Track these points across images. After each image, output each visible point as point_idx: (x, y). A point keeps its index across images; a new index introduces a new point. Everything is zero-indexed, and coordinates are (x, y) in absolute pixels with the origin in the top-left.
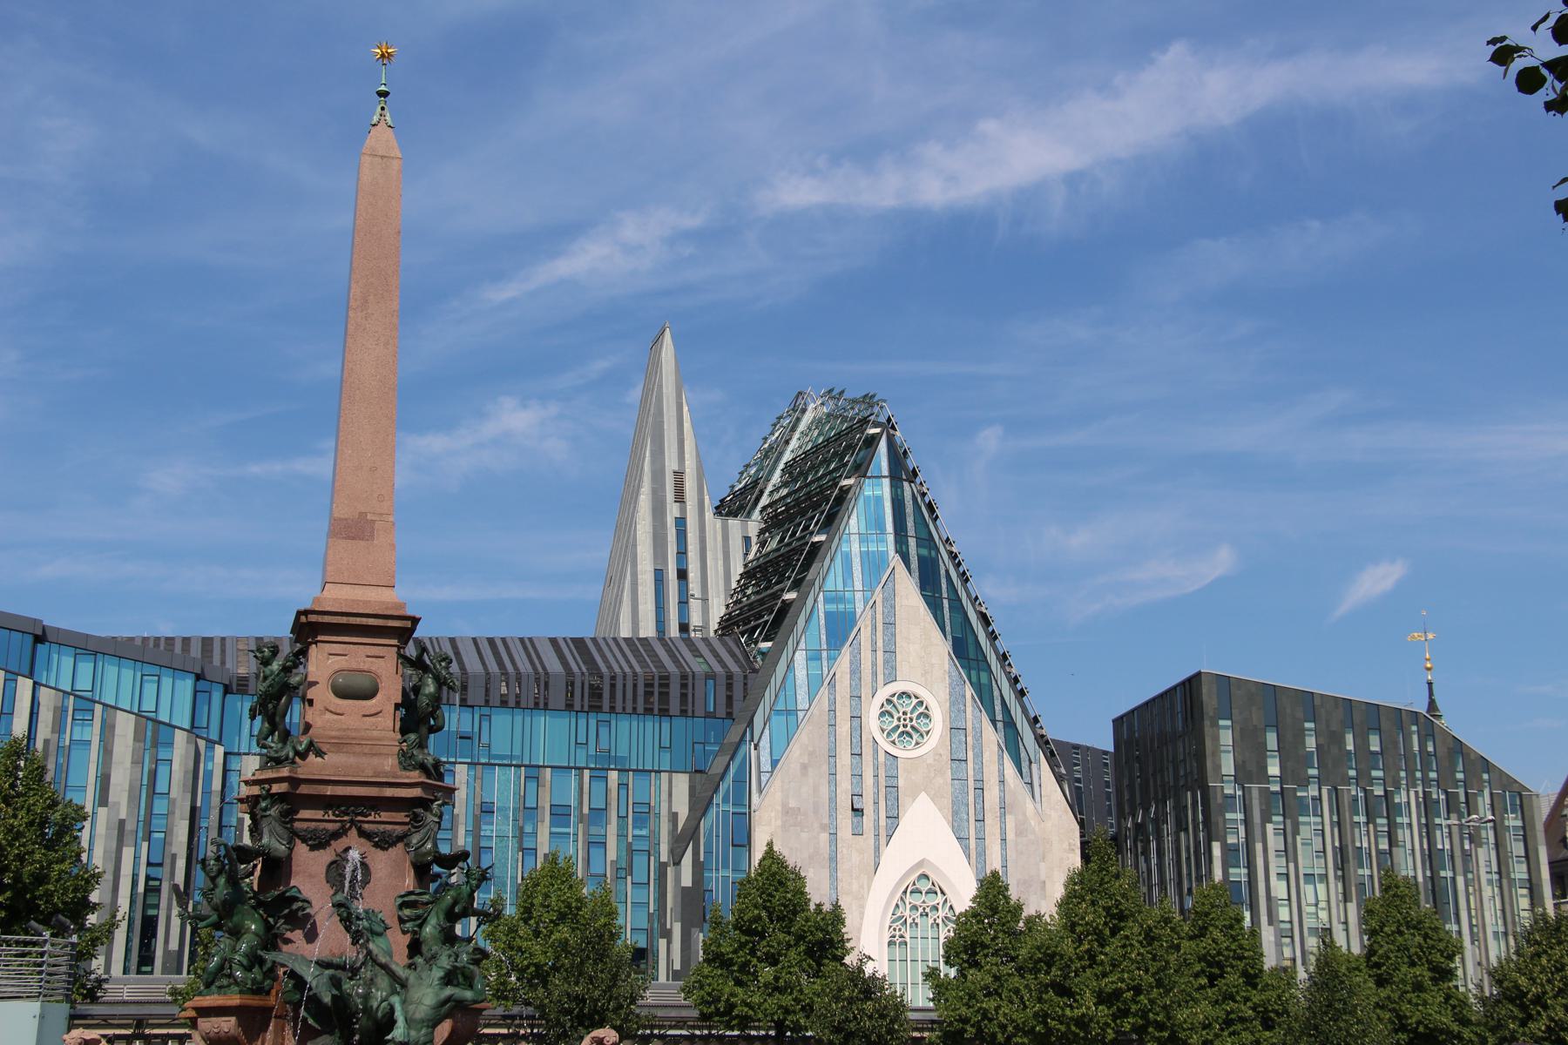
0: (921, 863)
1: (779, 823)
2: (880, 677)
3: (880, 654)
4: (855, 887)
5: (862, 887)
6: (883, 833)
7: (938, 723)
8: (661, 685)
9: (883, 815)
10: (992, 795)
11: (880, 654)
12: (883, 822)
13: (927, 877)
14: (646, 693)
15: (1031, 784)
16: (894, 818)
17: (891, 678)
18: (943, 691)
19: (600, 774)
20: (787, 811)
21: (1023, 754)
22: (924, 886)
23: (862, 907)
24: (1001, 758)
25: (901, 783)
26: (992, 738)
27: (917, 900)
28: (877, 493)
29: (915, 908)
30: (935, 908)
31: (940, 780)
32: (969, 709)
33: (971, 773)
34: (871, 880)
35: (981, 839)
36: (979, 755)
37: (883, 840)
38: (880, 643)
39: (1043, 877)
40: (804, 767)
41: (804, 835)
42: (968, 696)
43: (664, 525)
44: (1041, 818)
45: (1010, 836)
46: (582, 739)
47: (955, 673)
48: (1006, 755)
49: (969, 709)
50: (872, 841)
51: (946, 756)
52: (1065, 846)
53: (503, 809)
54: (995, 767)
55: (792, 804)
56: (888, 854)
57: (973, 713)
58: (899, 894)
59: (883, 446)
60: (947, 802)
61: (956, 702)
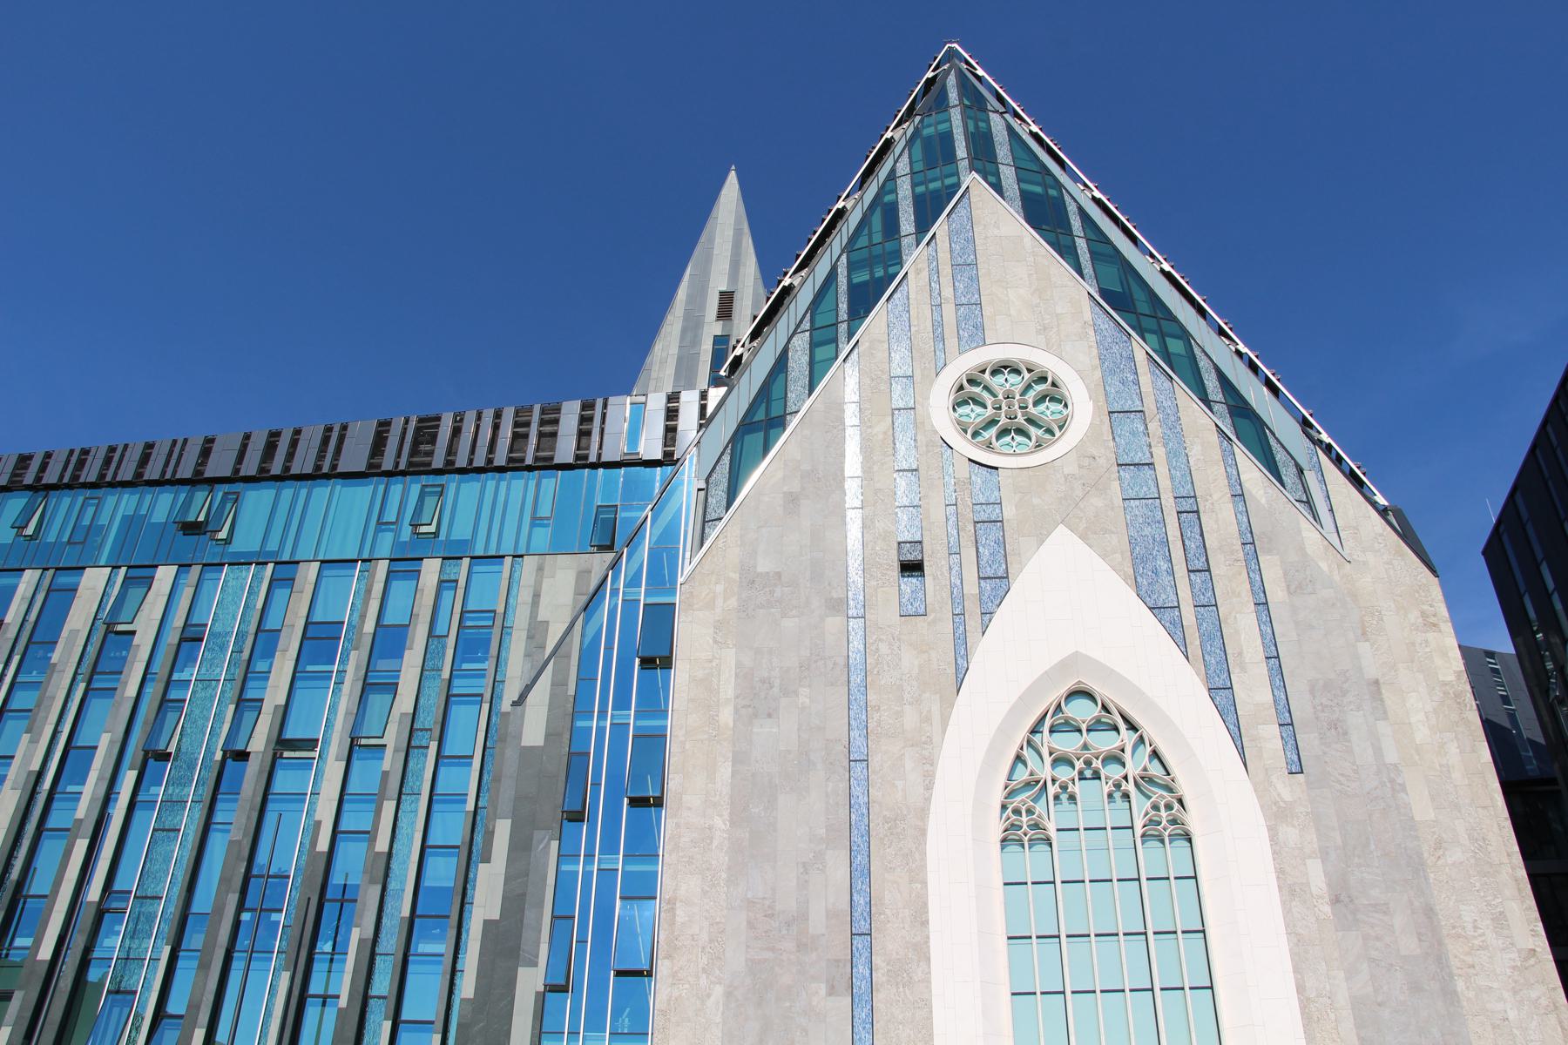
0: (1065, 665)
1: (733, 602)
2: (952, 342)
3: (949, 311)
4: (910, 718)
5: (927, 719)
6: (973, 609)
7: (1083, 409)
8: (542, 423)
9: (971, 574)
10: (1220, 521)
11: (949, 311)
12: (971, 586)
13: (1089, 695)
14: (516, 436)
15: (1309, 503)
16: (997, 581)
17: (976, 335)
18: (1087, 353)
19: (405, 565)
20: (750, 579)
21: (1280, 456)
22: (1082, 711)
23: (928, 765)
24: (1229, 459)
25: (1009, 512)
26: (1201, 425)
27: (1068, 743)
28: (942, 127)
29: (1061, 760)
30: (1115, 758)
31: (1096, 502)
32: (1145, 378)
33: (1165, 483)
34: (948, 706)
35: (1208, 605)
36: (1178, 453)
37: (973, 623)
38: (948, 292)
39: (1372, 672)
40: (792, 500)
41: (789, 624)
42: (1140, 356)
43: (696, 342)
44: (1336, 548)
45: (1276, 594)
46: (391, 516)
47: (1105, 324)
48: (1240, 451)
49: (1145, 378)
50: (948, 627)
51: (1105, 456)
52: (1414, 616)
53: (219, 638)
54: (1219, 471)
55: (764, 565)
56: (988, 652)
57: (1150, 381)
58: (1022, 734)
59: (952, 81)
60: (1118, 540)
61: (1114, 368)
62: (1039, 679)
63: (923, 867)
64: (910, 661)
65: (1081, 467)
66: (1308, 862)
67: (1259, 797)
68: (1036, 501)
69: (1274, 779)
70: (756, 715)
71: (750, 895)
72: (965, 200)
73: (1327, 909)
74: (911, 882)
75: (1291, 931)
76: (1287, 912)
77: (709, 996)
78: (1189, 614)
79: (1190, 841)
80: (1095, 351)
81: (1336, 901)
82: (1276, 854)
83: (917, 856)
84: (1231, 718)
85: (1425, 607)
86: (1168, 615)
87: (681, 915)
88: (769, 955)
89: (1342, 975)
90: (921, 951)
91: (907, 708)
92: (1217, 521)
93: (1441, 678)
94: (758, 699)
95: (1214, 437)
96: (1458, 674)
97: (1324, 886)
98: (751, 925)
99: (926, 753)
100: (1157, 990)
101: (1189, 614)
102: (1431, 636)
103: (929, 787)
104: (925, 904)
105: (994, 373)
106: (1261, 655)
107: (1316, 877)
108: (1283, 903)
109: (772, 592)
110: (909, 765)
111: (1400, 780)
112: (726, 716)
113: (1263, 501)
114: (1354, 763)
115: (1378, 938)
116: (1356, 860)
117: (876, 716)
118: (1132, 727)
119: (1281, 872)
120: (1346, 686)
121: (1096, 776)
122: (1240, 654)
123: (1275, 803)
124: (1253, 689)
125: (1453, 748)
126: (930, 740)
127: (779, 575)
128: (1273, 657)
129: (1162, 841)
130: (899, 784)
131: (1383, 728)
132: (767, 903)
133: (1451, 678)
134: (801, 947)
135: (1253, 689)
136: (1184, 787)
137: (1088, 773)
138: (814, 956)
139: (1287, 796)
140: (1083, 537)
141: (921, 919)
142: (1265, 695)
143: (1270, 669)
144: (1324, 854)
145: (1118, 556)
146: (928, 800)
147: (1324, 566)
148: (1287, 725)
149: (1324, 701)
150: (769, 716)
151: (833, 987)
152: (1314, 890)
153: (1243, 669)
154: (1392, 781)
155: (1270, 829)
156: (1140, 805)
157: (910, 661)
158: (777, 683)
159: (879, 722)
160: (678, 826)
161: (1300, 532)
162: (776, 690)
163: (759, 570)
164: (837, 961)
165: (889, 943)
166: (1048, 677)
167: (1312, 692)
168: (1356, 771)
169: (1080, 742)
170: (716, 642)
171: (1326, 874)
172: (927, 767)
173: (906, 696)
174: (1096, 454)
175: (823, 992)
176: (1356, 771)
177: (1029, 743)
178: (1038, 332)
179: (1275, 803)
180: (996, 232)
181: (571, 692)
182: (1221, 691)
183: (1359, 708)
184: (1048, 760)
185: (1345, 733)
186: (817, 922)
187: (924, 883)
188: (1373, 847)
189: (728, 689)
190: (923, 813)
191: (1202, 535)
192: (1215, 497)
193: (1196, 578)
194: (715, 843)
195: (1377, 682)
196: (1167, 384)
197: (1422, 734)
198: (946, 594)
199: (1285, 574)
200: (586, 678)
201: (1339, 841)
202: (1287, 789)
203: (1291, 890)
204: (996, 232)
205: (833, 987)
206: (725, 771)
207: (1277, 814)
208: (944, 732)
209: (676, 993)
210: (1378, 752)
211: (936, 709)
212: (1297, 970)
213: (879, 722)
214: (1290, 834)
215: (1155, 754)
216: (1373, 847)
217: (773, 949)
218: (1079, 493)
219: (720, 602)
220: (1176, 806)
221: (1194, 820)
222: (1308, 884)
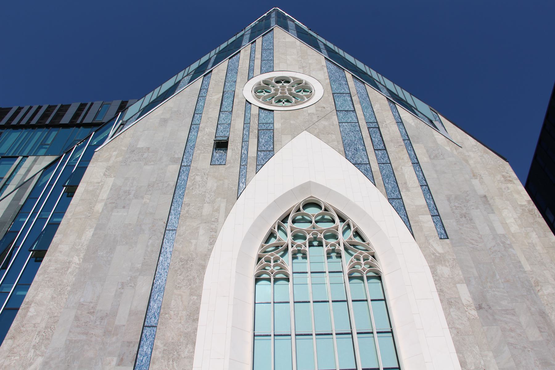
4: (207, 209)
5: (218, 210)
7: (319, 90)
10: (390, 131)
16: (266, 152)
17: (271, 69)
18: (324, 75)
22: (312, 211)
31: (324, 123)
34: (231, 204)
41: (148, 168)
45: (423, 159)
52: (499, 177)
60: (336, 136)
62: (289, 192)
63: (201, 286)
64: (211, 184)
65: (317, 110)
66: (458, 286)
67: (422, 251)
68: (292, 122)
69: (431, 241)
70: (116, 207)
71: (82, 300)
72: (271, 32)
73: (474, 313)
74: (191, 294)
75: (451, 325)
76: (448, 315)
77: (30, 364)
78: (375, 166)
79: (379, 278)
80: (327, 74)
81: (479, 308)
82: (437, 281)
83: (197, 280)
84: (402, 212)
85: (504, 174)
86: (363, 167)
87: (32, 311)
88: (84, 337)
89: (491, 354)
90: (190, 338)
91: (206, 205)
92: (389, 131)
93: (519, 203)
94: (119, 199)
95: (386, 102)
96: (528, 202)
97: (470, 299)
98: (77, 318)
99: (213, 226)
100: (272, 303)
101: (375, 166)
102: (510, 185)
103: (212, 243)
104: (198, 309)
105: (278, 82)
106: (417, 184)
107: (464, 294)
108: (444, 309)
109: (142, 155)
110: (201, 232)
111: (508, 242)
112: (99, 207)
113: (413, 124)
114: (479, 234)
115: (511, 330)
116: (489, 284)
117: (187, 208)
118: (342, 220)
119: (441, 292)
120: (467, 198)
121: (320, 245)
122: (406, 183)
123: (433, 254)
124: (414, 198)
125: (534, 235)
126: (217, 220)
127: (148, 149)
128: (425, 185)
129: (363, 280)
130: (194, 241)
131: (492, 217)
132: (92, 305)
133: (525, 203)
134: (107, 333)
135: (414, 198)
136: (376, 247)
137: (315, 243)
138: (114, 339)
139: (440, 249)
140: (317, 136)
141: (193, 316)
142: (422, 201)
143: (423, 191)
144: (468, 282)
145: (336, 143)
146: (210, 250)
147: (448, 148)
148: (436, 216)
149: (456, 204)
150: (124, 207)
151: (122, 360)
152: (465, 302)
153: (408, 189)
154: (503, 243)
155: (431, 267)
156: (347, 261)
157: (211, 184)
158: (133, 193)
159: (187, 212)
160: (50, 261)
161: (433, 136)
162: (131, 196)
163: (138, 146)
164: (129, 342)
165: (167, 333)
166: (292, 193)
167: (449, 200)
168: (481, 238)
169: (309, 227)
170: (105, 175)
171: (471, 293)
172: (213, 233)
173: (207, 199)
174: (324, 106)
175: (114, 363)
176: (481, 238)
177: (279, 228)
178: (299, 68)
179: (433, 254)
180: (284, 40)
181: (22, 203)
182: (396, 200)
183: (477, 208)
184: (289, 234)
185: (471, 220)
186: (122, 318)
187: (200, 296)
188: (498, 277)
189: (104, 195)
190: (206, 257)
191: (381, 136)
192: (387, 122)
193: (380, 153)
194: (70, 270)
195: (485, 196)
196: (362, 85)
197: (514, 228)
198: (238, 157)
199: (427, 151)
200: (32, 197)
201: (476, 274)
202: (439, 247)
203: (449, 303)
204: (284, 40)
205: (122, 360)
206: (89, 233)
207: (435, 261)
208: (226, 216)
209: (7, 363)
210: (492, 229)
211: (223, 206)
212: (458, 351)
213: (187, 212)
214: (444, 270)
215: (357, 234)
216: (498, 277)
217: (86, 334)
218: (315, 119)
219: (113, 159)
220: (371, 258)
221: (383, 266)
222: (459, 297)
